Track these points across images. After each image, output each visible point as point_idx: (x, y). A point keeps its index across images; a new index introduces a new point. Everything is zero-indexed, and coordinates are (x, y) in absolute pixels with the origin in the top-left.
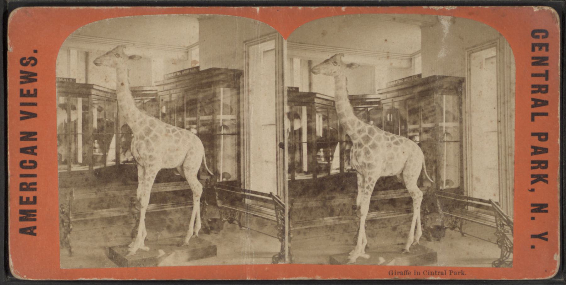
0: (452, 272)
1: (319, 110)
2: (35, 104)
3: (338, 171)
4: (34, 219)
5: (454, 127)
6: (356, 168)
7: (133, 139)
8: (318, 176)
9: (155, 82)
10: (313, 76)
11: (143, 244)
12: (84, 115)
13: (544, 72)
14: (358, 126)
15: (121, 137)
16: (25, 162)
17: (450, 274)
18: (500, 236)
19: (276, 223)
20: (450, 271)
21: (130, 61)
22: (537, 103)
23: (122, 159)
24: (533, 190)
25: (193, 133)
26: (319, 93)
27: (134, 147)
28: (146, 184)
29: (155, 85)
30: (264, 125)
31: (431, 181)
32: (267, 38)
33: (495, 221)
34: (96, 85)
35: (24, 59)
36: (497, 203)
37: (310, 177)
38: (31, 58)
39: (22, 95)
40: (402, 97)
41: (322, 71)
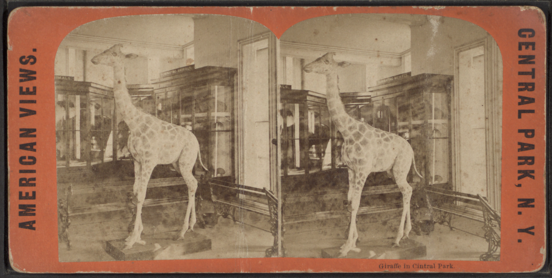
0: (440, 265)
1: (311, 108)
2: (34, 102)
3: (330, 167)
4: (33, 213)
6: (347, 163)
7: (130, 136)
8: (310, 172)
9: (152, 80)
12: (81, 112)
13: (530, 70)
14: (349, 123)
16: (24, 158)
17: (439, 268)
18: (487, 230)
19: (269, 218)
20: (439, 264)
21: (127, 59)
22: (524, 100)
23: (119, 155)
24: (519, 185)
26: (311, 90)
27: (131, 143)
28: (142, 180)
29: (151, 83)
33: (482, 216)
34: (93, 83)
35: (23, 57)
37: (302, 172)
38: (30, 57)
39: (22, 92)
40: (392, 95)
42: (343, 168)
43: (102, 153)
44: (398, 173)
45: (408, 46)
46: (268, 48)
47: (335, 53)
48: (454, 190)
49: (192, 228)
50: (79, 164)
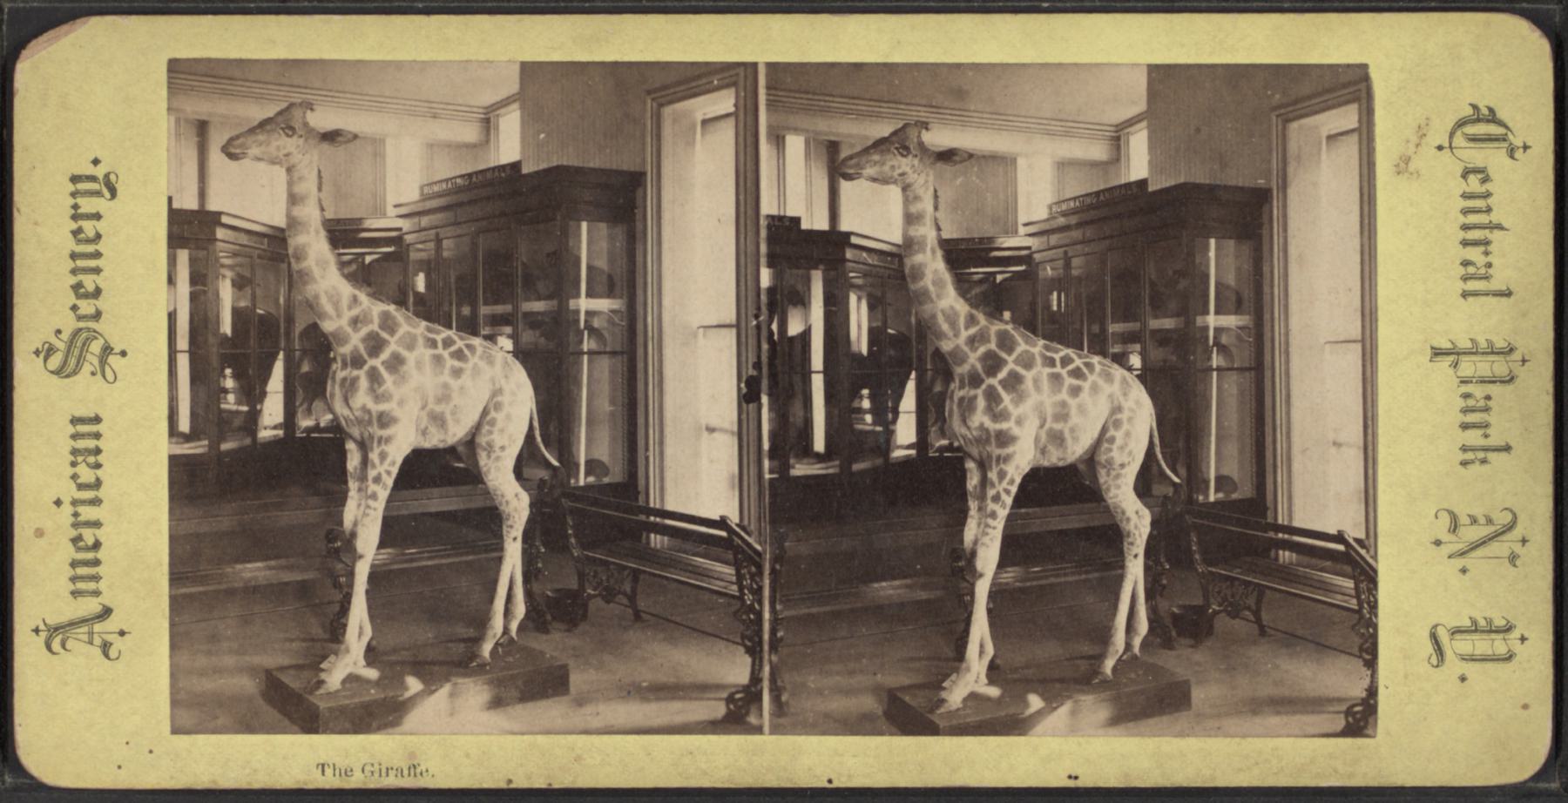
3: (280, 433)
5: (1240, 328)
6: (962, 442)
7: (334, 366)
8: (856, 467)
9: (396, 206)
10: (845, 187)
11: (984, 679)
12: (194, 297)
14: (350, 308)
15: (301, 360)
19: (737, 605)
21: (325, 146)
23: (305, 423)
25: (502, 348)
26: (860, 232)
27: (955, 408)
28: (369, 492)
29: (393, 215)
30: (1330, 342)
31: (1176, 480)
33: (1353, 592)
36: (1358, 541)
37: (830, 469)
40: (464, 226)
41: (254, 151)
42: (316, 435)
43: (253, 417)
44: (489, 452)
45: (1141, 106)
46: (735, 114)
47: (927, 123)
48: (1270, 520)
49: (1136, 650)
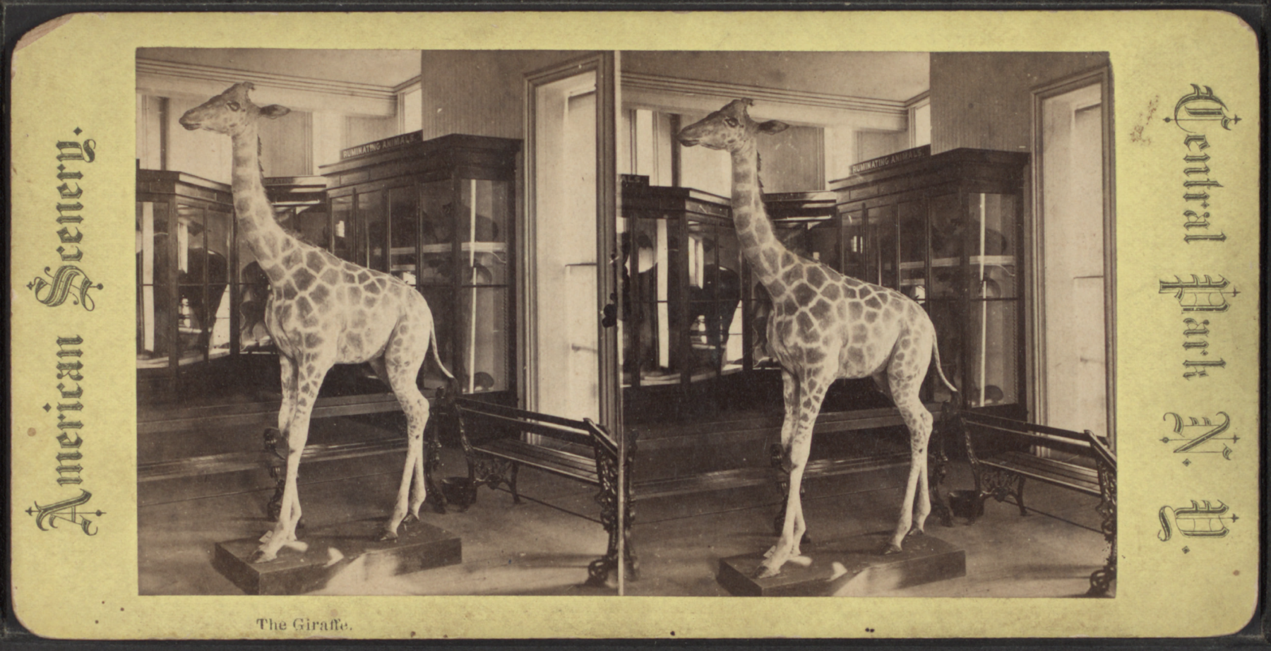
1: (184, 212)
3: (227, 351)
6: (780, 358)
7: (271, 297)
10: (685, 151)
11: (797, 551)
12: (157, 241)
14: (284, 250)
18: (1108, 514)
19: (597, 490)
21: (264, 118)
23: (247, 343)
25: (407, 282)
26: (186, 172)
27: (774, 330)
30: (1077, 278)
32: (577, 66)
33: (1097, 480)
34: (185, 174)
40: (376, 183)
41: (206, 122)
42: (256, 353)
43: (205, 338)
46: (596, 93)
47: (751, 100)
48: (1029, 421)
49: (921, 527)
50: (660, 380)
